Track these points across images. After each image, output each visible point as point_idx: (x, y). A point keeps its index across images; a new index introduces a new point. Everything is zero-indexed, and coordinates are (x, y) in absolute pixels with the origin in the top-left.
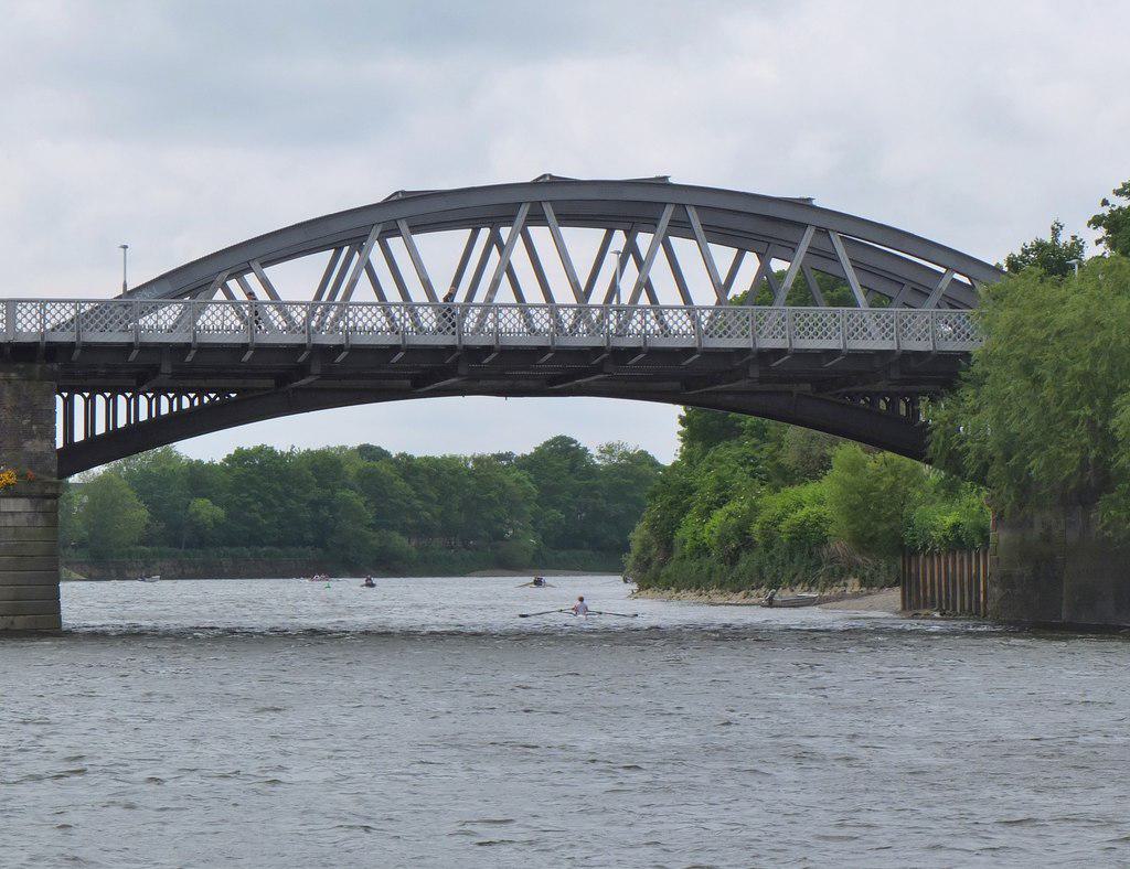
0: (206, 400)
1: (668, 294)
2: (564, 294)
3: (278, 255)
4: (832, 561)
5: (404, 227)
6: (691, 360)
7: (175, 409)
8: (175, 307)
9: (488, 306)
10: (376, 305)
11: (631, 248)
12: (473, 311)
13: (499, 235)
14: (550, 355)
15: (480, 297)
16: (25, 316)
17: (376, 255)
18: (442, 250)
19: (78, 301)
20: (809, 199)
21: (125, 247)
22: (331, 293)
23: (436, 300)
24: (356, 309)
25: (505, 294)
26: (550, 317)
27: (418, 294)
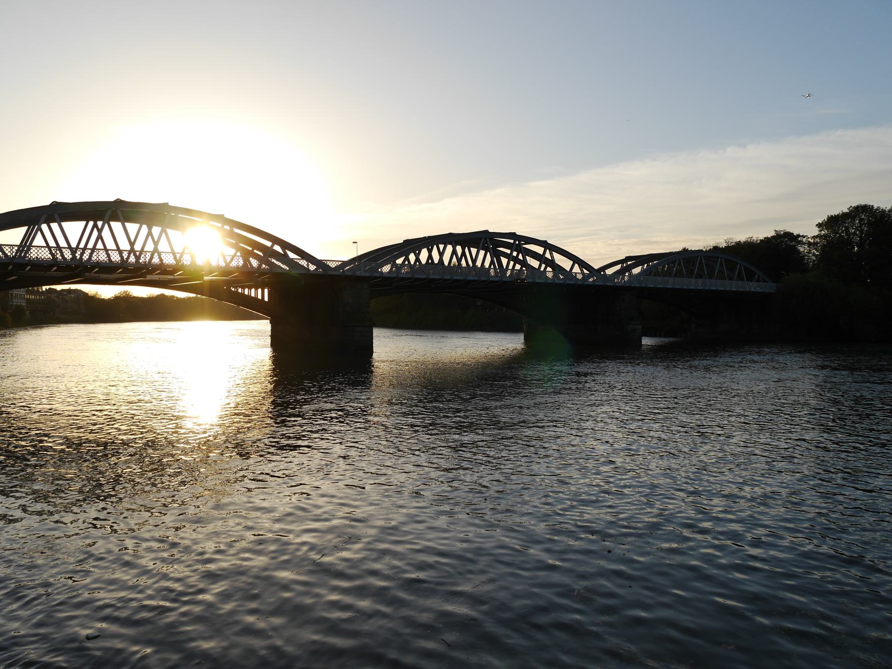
0: (412, 257)
1: (111, 245)
2: (125, 245)
4: (852, 476)
5: (121, 217)
8: (389, 265)
9: (93, 249)
10: (170, 253)
11: (150, 234)
13: (97, 225)
14: (97, 269)
15: (90, 245)
17: (44, 227)
18: (74, 229)
19: (12, 245)
22: (27, 241)
24: (34, 249)
26: (56, 256)
27: (63, 243)
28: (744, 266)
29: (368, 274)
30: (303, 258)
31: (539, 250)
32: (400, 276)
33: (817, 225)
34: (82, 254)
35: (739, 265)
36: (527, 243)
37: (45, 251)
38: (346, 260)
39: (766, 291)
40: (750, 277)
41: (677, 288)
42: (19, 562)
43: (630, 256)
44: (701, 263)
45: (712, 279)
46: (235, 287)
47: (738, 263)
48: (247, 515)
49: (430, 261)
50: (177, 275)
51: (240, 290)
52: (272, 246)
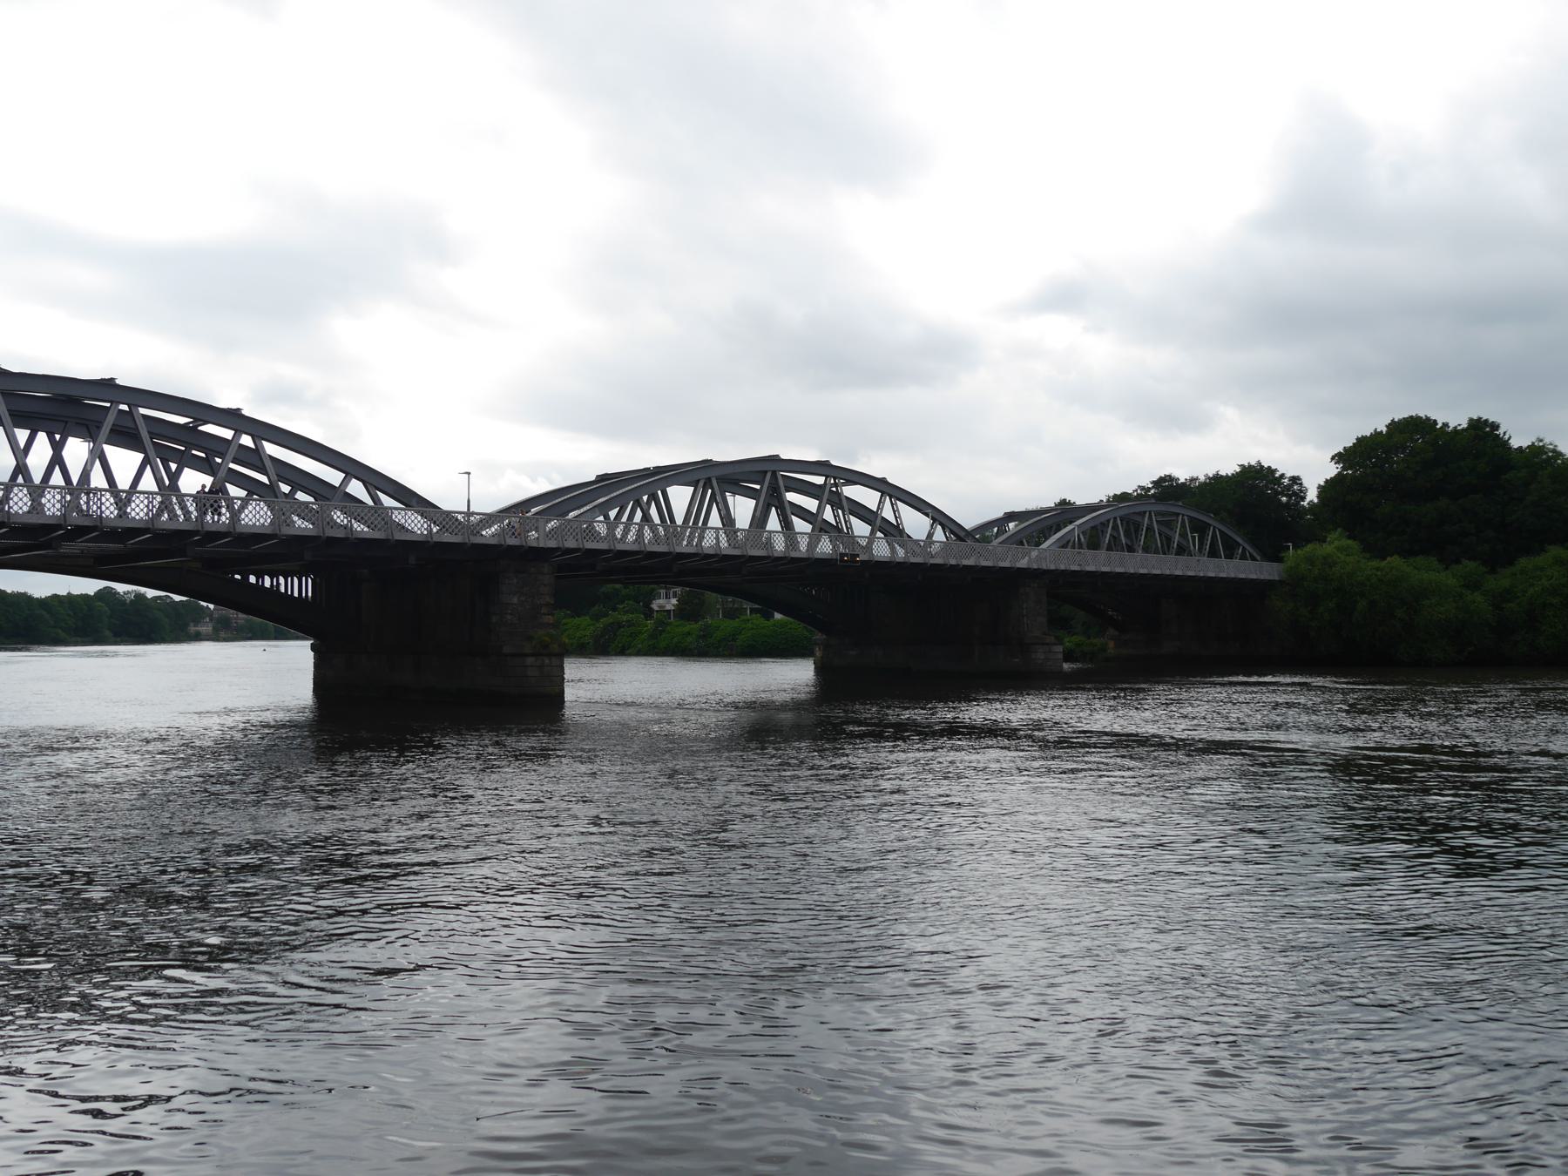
3: (10, 436)
6: (91, 535)
7: (289, 579)
12: (49, 492)
14: (97, 533)
16: (138, 506)
20: (239, 409)
21: (469, 473)
23: (71, 483)
25: (801, 525)
28: (1219, 530)
29: (552, 544)
30: (408, 506)
31: (333, 477)
32: (239, 530)
33: (1333, 458)
34: (626, 531)
35: (1212, 528)
36: (850, 482)
37: (20, 495)
38: (489, 511)
39: (1262, 577)
40: (1231, 550)
41: (1074, 571)
42: (968, 942)
43: (1013, 512)
44: (1150, 528)
45: (1147, 552)
46: (259, 576)
47: (1210, 525)
48: (754, 980)
49: (58, 437)
50: (132, 544)
51: (267, 582)
52: (345, 482)
